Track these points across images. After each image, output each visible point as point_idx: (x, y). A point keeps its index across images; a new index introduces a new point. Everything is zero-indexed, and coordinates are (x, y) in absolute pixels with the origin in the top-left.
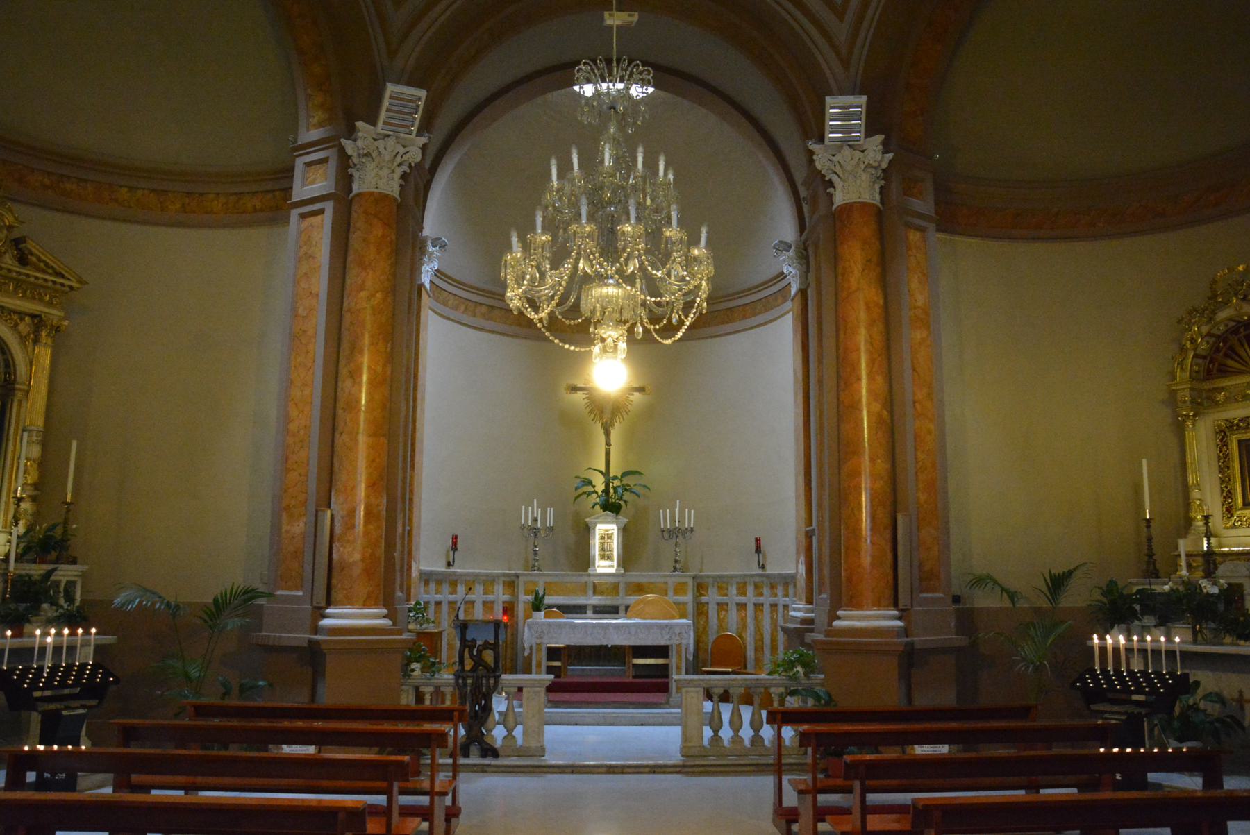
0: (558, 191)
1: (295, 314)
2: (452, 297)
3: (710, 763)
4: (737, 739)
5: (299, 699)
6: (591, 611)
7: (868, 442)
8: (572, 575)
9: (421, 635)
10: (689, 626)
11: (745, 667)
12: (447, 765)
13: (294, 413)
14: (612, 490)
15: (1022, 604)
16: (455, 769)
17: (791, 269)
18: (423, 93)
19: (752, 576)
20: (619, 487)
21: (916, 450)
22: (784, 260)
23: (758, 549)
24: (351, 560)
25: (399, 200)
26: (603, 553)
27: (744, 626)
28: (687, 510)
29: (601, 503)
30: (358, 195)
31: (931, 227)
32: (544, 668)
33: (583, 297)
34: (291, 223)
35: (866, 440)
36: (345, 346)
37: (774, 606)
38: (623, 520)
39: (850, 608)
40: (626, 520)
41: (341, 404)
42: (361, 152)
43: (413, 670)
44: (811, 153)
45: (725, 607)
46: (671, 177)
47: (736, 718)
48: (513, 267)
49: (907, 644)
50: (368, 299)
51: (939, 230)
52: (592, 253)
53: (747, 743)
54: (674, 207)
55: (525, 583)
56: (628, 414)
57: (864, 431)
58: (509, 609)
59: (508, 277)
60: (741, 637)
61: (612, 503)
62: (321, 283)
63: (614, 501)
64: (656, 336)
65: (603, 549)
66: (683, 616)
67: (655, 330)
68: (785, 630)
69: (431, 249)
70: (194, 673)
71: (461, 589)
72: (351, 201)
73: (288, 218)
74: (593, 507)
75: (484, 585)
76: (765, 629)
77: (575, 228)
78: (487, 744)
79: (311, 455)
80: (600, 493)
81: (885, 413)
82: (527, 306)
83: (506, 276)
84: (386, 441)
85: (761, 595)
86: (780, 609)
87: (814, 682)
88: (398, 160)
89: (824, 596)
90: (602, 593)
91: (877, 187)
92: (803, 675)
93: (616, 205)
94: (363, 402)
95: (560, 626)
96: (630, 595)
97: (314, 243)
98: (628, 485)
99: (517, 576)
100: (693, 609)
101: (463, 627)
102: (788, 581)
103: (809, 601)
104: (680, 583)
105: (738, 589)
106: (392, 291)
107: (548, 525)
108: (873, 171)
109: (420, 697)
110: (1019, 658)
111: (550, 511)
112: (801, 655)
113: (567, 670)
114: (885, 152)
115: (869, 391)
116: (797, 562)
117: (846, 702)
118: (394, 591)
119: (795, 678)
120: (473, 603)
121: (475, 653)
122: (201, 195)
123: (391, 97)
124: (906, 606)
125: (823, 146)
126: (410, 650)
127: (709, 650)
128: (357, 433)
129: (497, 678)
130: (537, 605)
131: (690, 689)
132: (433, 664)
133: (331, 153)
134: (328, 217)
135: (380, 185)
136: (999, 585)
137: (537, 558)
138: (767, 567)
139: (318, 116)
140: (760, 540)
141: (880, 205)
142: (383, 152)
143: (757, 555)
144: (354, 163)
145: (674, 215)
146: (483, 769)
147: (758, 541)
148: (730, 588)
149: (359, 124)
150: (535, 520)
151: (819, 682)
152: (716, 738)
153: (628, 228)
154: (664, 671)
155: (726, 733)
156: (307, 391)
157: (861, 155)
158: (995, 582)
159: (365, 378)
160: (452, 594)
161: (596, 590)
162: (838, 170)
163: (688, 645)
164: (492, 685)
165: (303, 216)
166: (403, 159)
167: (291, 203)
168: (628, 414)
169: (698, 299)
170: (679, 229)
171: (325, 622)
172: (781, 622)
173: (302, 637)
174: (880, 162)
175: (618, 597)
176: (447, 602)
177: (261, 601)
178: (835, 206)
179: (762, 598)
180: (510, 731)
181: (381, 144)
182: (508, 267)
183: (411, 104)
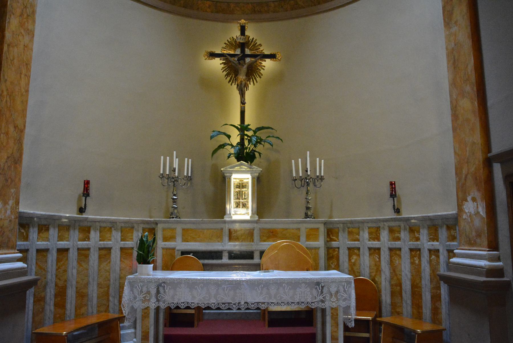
6: (227, 257)
10: (348, 282)
23: (393, 195)
27: (378, 270)
38: (257, 170)
45: (398, 252)
55: (164, 230)
56: (260, 77)
60: (373, 280)
71: (94, 235)
74: (229, 157)
75: (122, 232)
76: (403, 274)
85: (398, 239)
90: (237, 239)
96: (264, 241)
99: (156, 223)
100: (325, 254)
104: (312, 229)
105: (370, 233)
107: (185, 174)
111: (188, 162)
120: (109, 249)
140: (394, 184)
143: (392, 199)
147: (392, 184)
148: (361, 233)
160: (84, 240)
161: (232, 236)
168: (260, 77)
175: (253, 243)
179: (399, 242)
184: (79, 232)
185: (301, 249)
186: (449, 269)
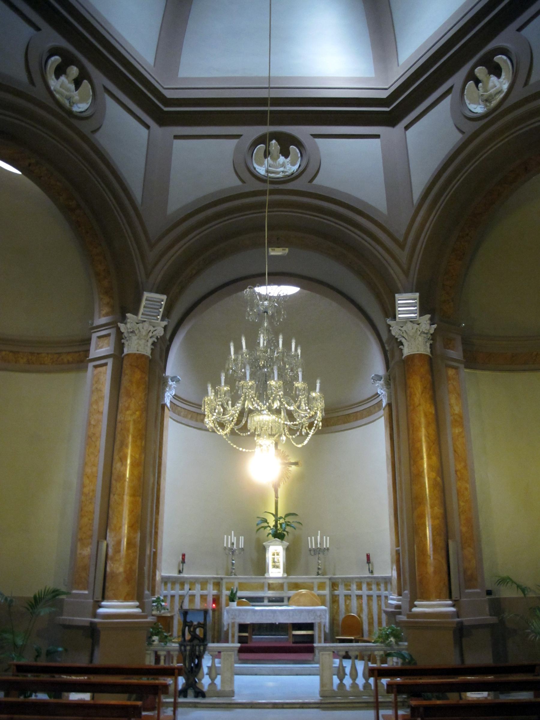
0: (234, 360)
1: (89, 423)
2: (183, 410)
3: (339, 701)
4: (354, 685)
5: (82, 661)
7: (429, 496)
8: (255, 578)
9: (160, 618)
10: (325, 610)
11: (363, 636)
12: (170, 703)
13: (87, 481)
14: (279, 526)
15: (531, 595)
16: (175, 705)
17: (382, 391)
18: (164, 297)
19: (365, 578)
20: (283, 523)
21: (458, 500)
22: (378, 386)
24: (118, 572)
25: (150, 357)
26: (274, 564)
28: (325, 537)
29: (272, 533)
30: (127, 355)
31: (462, 366)
32: (236, 638)
33: (249, 421)
34: (88, 371)
35: (428, 495)
36: (118, 443)
37: (379, 597)
38: (286, 543)
39: (422, 600)
40: (288, 544)
41: (114, 477)
42: (129, 330)
43: (154, 641)
44: (389, 326)
45: (349, 597)
46: (299, 351)
47: (354, 673)
48: (208, 404)
49: (458, 623)
50: (131, 415)
51: (466, 367)
52: (252, 398)
53: (361, 688)
54: (300, 369)
55: (227, 583)
57: (426, 490)
58: (216, 600)
59: (206, 410)
61: (279, 533)
62: (105, 406)
63: (280, 532)
64: (293, 442)
65: (274, 562)
66: (323, 604)
67: (292, 438)
68: (386, 613)
69: (170, 383)
70: (20, 642)
71: (187, 587)
72: (123, 358)
73: (87, 367)
74: (268, 536)
77: (243, 383)
78: (198, 689)
79: (96, 507)
80: (272, 527)
81: (439, 479)
82: (217, 426)
83: (204, 410)
84: (140, 500)
86: (383, 598)
87: (402, 647)
88: (150, 334)
89: (406, 592)
90: (273, 589)
91: (428, 345)
92: (394, 643)
93: (267, 368)
94: (128, 476)
95: (247, 611)
96: (291, 590)
97: (101, 383)
98: (289, 522)
99: (222, 579)
101: (185, 613)
102: (387, 581)
103: (400, 594)
105: (357, 586)
106: (146, 409)
108: (425, 336)
109: (157, 659)
110: (529, 631)
111: (242, 539)
112: (393, 630)
113: (252, 638)
114: (432, 324)
115: (429, 466)
116: (392, 569)
117: (423, 663)
118: (143, 592)
119: (389, 645)
121: (192, 629)
122: (38, 354)
123: (146, 300)
124: (456, 598)
125: (394, 322)
126: (153, 628)
127: (340, 624)
128: (123, 495)
129: (205, 646)
130: (232, 598)
131: (324, 652)
132: (166, 637)
133: (112, 331)
134: (109, 368)
135: (140, 348)
136: (516, 583)
137: (234, 568)
138: (374, 572)
139: (106, 310)
141: (430, 355)
142: (142, 330)
143: (368, 565)
144: (125, 337)
145: (300, 374)
146: (195, 706)
147: (368, 556)
149: (128, 315)
150: (233, 544)
151: (404, 647)
152: (341, 685)
153: (273, 383)
154: (311, 639)
155: (348, 681)
156: (95, 469)
157: (418, 326)
158: (513, 582)
159: (129, 462)
161: (270, 587)
162: (405, 335)
163: (325, 623)
164: (202, 651)
165: (96, 367)
166: (153, 334)
167: (89, 359)
169: (316, 422)
170: (303, 382)
171: (101, 610)
172: (384, 607)
173: (85, 620)
174: (429, 330)
176: (178, 596)
177: (63, 597)
178: (403, 357)
180: (213, 679)
181: (140, 325)
182: (206, 404)
183: (156, 310)
184: (213, 587)
185: (314, 596)
186: (387, 607)
